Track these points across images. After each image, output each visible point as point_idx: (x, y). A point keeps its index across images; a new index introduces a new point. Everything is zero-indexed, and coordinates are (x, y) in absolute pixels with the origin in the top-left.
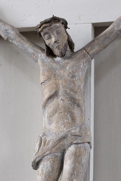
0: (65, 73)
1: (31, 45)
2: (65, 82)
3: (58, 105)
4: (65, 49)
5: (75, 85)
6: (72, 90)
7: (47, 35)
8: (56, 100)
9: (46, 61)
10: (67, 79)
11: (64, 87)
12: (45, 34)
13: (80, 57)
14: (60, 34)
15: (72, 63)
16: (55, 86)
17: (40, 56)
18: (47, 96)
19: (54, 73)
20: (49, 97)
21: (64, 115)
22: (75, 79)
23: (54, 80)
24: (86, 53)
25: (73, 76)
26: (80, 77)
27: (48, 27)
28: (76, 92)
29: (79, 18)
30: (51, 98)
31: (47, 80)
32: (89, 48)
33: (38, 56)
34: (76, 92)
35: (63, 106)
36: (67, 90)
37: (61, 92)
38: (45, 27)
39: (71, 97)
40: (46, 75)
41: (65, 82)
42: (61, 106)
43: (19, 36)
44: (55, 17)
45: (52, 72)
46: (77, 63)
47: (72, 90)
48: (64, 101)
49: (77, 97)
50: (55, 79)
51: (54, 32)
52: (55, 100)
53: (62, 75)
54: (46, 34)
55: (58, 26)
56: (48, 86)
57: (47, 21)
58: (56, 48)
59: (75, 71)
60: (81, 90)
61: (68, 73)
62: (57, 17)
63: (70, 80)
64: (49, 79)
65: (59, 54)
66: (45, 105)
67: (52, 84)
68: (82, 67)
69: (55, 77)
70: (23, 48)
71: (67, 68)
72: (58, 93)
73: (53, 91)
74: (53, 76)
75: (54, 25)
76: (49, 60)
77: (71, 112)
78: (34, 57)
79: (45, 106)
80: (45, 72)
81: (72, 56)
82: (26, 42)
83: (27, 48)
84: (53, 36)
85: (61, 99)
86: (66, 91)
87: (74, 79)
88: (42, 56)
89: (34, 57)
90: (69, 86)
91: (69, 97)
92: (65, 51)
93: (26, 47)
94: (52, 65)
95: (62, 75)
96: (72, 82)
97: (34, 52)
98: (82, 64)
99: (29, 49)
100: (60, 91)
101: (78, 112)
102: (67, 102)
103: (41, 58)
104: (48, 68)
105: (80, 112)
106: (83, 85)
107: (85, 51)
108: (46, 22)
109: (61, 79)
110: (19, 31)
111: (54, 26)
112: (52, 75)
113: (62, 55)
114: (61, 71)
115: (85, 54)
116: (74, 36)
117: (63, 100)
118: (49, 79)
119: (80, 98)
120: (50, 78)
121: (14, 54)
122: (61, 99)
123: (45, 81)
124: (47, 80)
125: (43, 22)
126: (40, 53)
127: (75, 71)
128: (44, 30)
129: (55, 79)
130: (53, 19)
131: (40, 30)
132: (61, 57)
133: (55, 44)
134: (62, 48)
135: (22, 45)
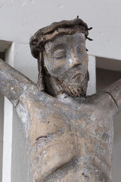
7: (59, 51)
8: (71, 174)
10: (95, 138)
11: (89, 151)
16: (72, 146)
17: (25, 88)
18: (53, 163)
20: (58, 166)
22: (107, 141)
27: (68, 36)
32: (117, 93)
33: (23, 89)
36: (96, 158)
37: (82, 161)
40: (52, 124)
41: (91, 143)
48: (88, 177)
50: (71, 134)
52: (70, 173)
53: (85, 129)
54: (59, 48)
56: (57, 146)
58: (74, 77)
61: (96, 127)
62: (48, 25)
65: (76, 91)
69: (70, 130)
72: (76, 162)
73: (68, 157)
76: (50, 99)
78: (12, 89)
86: (94, 159)
89: (70, 87)
91: (98, 173)
94: (59, 108)
95: (85, 129)
97: (12, 79)
100: (82, 158)
107: (110, 97)
108: (65, 25)
109: (83, 136)
111: (78, 36)
113: (82, 94)
114: (80, 122)
117: (86, 176)
120: (61, 131)
123: (49, 134)
124: (55, 133)
126: (27, 83)
129: (72, 135)
130: (79, 22)
131: (48, 37)
133: (73, 71)
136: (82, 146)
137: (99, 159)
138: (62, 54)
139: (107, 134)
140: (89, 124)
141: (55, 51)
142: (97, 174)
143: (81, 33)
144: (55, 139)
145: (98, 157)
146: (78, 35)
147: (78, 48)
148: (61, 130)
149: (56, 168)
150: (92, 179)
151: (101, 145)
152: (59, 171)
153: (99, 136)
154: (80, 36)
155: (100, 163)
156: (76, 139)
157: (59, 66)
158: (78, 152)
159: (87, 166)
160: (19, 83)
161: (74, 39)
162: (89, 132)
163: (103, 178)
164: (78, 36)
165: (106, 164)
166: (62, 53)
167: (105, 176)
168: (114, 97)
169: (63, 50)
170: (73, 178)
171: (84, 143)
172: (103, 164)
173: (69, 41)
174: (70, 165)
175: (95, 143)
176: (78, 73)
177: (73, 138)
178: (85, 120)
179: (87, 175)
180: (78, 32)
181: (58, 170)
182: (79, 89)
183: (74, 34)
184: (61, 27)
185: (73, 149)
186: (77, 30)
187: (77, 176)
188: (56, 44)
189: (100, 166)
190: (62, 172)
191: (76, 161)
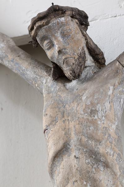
0: (78, 109)
1: (31, 65)
2: (78, 124)
3: (71, 167)
4: (80, 63)
5: (96, 128)
6: (91, 137)
7: (46, 42)
8: (66, 159)
9: (53, 89)
10: (83, 118)
11: (77, 134)
12: (44, 38)
13: (108, 75)
14: (67, 37)
15: (92, 87)
16: (64, 133)
18: (51, 153)
19: (62, 108)
20: (54, 155)
21: (82, 184)
23: (62, 123)
24: (121, 66)
25: (93, 112)
26: (106, 112)
27: (45, 27)
28: (99, 141)
29: (120, 5)
30: (58, 155)
31: (51, 124)
33: (43, 83)
34: (99, 141)
35: (78, 169)
36: (83, 137)
38: (40, 27)
39: (91, 151)
40: (49, 115)
42: (74, 170)
43: (12, 51)
44: (55, 5)
45: (59, 109)
46: (102, 86)
47: (92, 138)
48: (79, 158)
49: (101, 149)
51: (56, 35)
52: (65, 158)
54: (45, 40)
55: (62, 23)
57: (41, 16)
59: (96, 102)
60: (110, 135)
61: (84, 106)
63: (88, 119)
64: (54, 122)
66: (52, 171)
67: (59, 129)
68: (110, 92)
69: (63, 117)
70: (19, 70)
71: (84, 98)
72: (68, 146)
73: (61, 143)
74: (60, 115)
75: (54, 21)
77: (93, 178)
78: (37, 85)
79: (52, 173)
80: (49, 109)
81: (95, 75)
82: (23, 59)
83: (24, 70)
84: (55, 42)
85: (75, 156)
87: (94, 116)
88: (47, 81)
89: (37, 85)
90: (87, 130)
92: (79, 67)
93: (24, 68)
96: (90, 122)
97: (35, 76)
98: (112, 88)
99: (28, 73)
101: (108, 178)
102: (85, 161)
103: (47, 86)
104: (52, 103)
105: (111, 177)
106: (114, 127)
108: (41, 18)
110: (15, 43)
111: (55, 23)
112: (60, 112)
115: (118, 68)
116: (112, 39)
117: (77, 158)
118: (53, 121)
119: (108, 150)
121: (20, 88)
122: (75, 156)
125: (36, 19)
127: (96, 102)
128: (39, 33)
129: (64, 121)
132: (74, 79)
133: (60, 57)
134: (74, 62)
135: (17, 66)
136: (72, 130)
137: (86, 138)
138: (49, 45)
139: (95, 110)
140: (79, 105)
141: (43, 43)
142: (86, 153)
143: (60, 18)
144: (51, 129)
145: (85, 136)
146: (54, 22)
147: (61, 33)
148: (55, 119)
149: (53, 158)
150: (82, 159)
151: (88, 123)
152: (57, 159)
153: (86, 114)
154: (58, 22)
155: (86, 142)
156: (67, 125)
157: (51, 56)
158: (69, 136)
159: (77, 148)
160: (40, 78)
161: (52, 28)
162: (79, 113)
163: (92, 155)
164: (56, 23)
165: (94, 141)
166: (49, 44)
167: (93, 152)
168: (121, 62)
169: (48, 40)
170: (68, 163)
171: (73, 126)
172: (90, 141)
173: (48, 31)
174: (63, 152)
175: (82, 123)
176: (64, 58)
177: (65, 124)
178: (77, 102)
179: (78, 156)
180: (53, 19)
181: (55, 159)
182: (71, 72)
183: (49, 23)
184: (38, 21)
185: (64, 135)
186: (51, 19)
187: (71, 159)
188: (40, 37)
189: (87, 145)
190: (59, 159)
191: (68, 146)
